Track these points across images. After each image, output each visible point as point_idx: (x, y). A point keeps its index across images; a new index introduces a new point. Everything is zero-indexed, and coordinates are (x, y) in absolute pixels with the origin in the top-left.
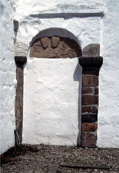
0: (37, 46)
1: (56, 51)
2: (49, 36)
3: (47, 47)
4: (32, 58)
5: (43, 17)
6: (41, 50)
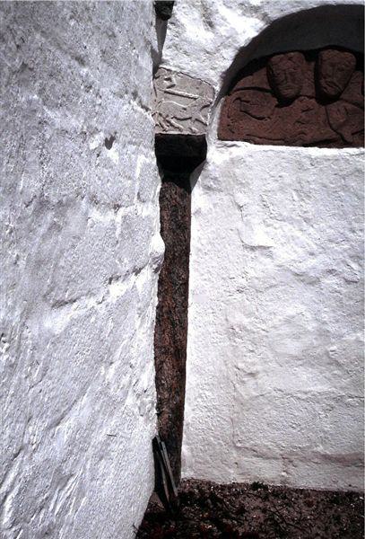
2: (305, 49)
3: (297, 96)
4: (230, 143)
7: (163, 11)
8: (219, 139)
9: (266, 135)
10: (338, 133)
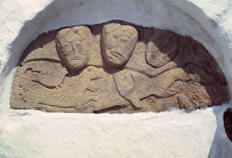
1: (122, 83)
4: (22, 111)
6: (60, 81)
8: (12, 108)
9: (57, 103)
10: (127, 100)
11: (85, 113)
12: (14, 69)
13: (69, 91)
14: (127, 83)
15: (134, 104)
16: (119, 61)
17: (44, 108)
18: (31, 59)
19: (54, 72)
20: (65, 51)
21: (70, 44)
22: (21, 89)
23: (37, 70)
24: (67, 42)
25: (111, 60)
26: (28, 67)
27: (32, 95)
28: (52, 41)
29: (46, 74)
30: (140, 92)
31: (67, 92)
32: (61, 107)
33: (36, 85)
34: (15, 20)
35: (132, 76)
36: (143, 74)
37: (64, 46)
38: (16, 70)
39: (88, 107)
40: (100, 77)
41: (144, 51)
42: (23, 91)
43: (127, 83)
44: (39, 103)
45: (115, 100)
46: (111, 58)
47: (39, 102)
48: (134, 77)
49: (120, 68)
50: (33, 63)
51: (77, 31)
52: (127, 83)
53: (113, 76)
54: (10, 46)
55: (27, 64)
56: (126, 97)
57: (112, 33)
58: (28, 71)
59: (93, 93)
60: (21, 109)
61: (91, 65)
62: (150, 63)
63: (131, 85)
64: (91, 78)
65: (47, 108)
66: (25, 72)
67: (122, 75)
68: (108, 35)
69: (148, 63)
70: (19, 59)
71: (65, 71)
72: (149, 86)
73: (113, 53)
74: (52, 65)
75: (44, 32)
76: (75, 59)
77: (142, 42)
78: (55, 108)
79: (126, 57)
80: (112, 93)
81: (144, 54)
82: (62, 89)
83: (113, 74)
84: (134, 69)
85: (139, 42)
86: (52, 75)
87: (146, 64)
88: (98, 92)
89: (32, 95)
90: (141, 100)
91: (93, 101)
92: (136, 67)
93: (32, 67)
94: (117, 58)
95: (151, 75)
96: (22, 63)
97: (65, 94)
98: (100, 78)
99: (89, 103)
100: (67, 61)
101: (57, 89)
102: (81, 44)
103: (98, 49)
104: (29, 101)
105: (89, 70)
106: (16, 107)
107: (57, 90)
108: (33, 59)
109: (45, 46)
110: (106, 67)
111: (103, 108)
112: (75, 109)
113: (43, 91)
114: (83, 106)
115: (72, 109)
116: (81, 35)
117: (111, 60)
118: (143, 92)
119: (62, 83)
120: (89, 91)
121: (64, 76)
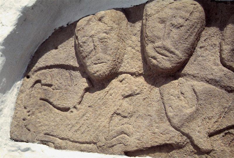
0: (56, 70)
1: (176, 103)
2: (126, 6)
3: (113, 74)
4: (24, 145)
5: (35, 6)
6: (77, 99)
7: (230, 90)
8: (12, 139)
9: (70, 135)
10: (184, 134)
11: (111, 154)
12: (19, 82)
13: (89, 115)
14: (183, 103)
15: (196, 142)
16: (168, 62)
17: (51, 142)
18: (41, 66)
19: (69, 86)
20: (82, 50)
21: (91, 39)
22: (25, 111)
23: (47, 83)
24: (87, 36)
25: (154, 61)
26: (37, 79)
27: (38, 120)
28: (71, 37)
29: (59, 88)
30: (207, 120)
31: (85, 118)
32: (76, 142)
33: (44, 105)
34: (11, 9)
35: (194, 90)
36: (215, 85)
37: (81, 44)
38: (21, 83)
39: (115, 145)
40: (137, 92)
41: (217, 43)
42: (28, 114)
43: (184, 102)
44: (45, 134)
45: (162, 133)
46: (154, 58)
47: (45, 132)
48: (197, 91)
49: (173, 76)
50: (43, 73)
51: (102, 17)
52: (183, 103)
53: (160, 91)
54: (2, 46)
55: (36, 74)
56: (182, 129)
57: (157, 15)
58: (37, 84)
59: (125, 120)
60: (22, 141)
61: (125, 73)
62: (228, 63)
63: (191, 107)
64: (123, 94)
65: (56, 142)
66: (32, 86)
67: (174, 88)
68: (150, 19)
69: (224, 65)
70: (26, 68)
71: (84, 84)
72: (226, 109)
73: (157, 49)
74: (68, 74)
75: (61, 26)
76: (97, 62)
77: (214, 26)
78: (67, 143)
79: (180, 55)
80: (157, 121)
81: (217, 49)
82: (78, 112)
83: (160, 86)
84: (198, 77)
85: (208, 27)
86: (66, 89)
87: (221, 66)
88: (133, 119)
89: (38, 120)
90: (211, 135)
91: (125, 134)
92: (202, 74)
93: (41, 78)
94: (164, 57)
95: (230, 87)
96: (30, 74)
97: (82, 121)
98: (138, 94)
99: (117, 137)
100: (86, 67)
101: (72, 112)
102: (106, 37)
103: (137, 46)
104: (33, 130)
105: (121, 81)
106: (16, 137)
107: (72, 114)
108: (44, 66)
109: (60, 46)
110: (149, 76)
111: (140, 147)
112: (95, 146)
113: (52, 115)
114: (108, 142)
115: (90, 146)
116: (106, 24)
117: (154, 61)
118: (214, 120)
119: (80, 103)
120: (119, 117)
121: (82, 92)
